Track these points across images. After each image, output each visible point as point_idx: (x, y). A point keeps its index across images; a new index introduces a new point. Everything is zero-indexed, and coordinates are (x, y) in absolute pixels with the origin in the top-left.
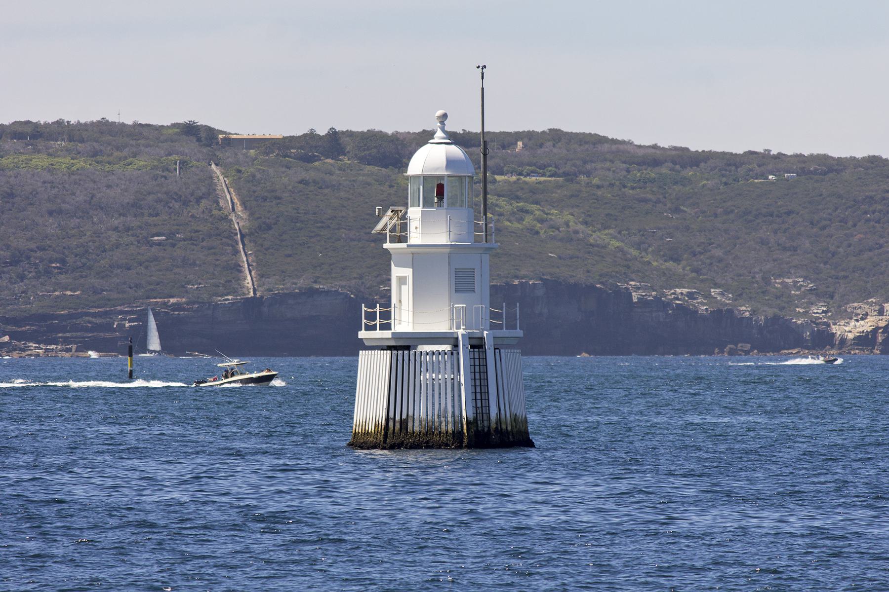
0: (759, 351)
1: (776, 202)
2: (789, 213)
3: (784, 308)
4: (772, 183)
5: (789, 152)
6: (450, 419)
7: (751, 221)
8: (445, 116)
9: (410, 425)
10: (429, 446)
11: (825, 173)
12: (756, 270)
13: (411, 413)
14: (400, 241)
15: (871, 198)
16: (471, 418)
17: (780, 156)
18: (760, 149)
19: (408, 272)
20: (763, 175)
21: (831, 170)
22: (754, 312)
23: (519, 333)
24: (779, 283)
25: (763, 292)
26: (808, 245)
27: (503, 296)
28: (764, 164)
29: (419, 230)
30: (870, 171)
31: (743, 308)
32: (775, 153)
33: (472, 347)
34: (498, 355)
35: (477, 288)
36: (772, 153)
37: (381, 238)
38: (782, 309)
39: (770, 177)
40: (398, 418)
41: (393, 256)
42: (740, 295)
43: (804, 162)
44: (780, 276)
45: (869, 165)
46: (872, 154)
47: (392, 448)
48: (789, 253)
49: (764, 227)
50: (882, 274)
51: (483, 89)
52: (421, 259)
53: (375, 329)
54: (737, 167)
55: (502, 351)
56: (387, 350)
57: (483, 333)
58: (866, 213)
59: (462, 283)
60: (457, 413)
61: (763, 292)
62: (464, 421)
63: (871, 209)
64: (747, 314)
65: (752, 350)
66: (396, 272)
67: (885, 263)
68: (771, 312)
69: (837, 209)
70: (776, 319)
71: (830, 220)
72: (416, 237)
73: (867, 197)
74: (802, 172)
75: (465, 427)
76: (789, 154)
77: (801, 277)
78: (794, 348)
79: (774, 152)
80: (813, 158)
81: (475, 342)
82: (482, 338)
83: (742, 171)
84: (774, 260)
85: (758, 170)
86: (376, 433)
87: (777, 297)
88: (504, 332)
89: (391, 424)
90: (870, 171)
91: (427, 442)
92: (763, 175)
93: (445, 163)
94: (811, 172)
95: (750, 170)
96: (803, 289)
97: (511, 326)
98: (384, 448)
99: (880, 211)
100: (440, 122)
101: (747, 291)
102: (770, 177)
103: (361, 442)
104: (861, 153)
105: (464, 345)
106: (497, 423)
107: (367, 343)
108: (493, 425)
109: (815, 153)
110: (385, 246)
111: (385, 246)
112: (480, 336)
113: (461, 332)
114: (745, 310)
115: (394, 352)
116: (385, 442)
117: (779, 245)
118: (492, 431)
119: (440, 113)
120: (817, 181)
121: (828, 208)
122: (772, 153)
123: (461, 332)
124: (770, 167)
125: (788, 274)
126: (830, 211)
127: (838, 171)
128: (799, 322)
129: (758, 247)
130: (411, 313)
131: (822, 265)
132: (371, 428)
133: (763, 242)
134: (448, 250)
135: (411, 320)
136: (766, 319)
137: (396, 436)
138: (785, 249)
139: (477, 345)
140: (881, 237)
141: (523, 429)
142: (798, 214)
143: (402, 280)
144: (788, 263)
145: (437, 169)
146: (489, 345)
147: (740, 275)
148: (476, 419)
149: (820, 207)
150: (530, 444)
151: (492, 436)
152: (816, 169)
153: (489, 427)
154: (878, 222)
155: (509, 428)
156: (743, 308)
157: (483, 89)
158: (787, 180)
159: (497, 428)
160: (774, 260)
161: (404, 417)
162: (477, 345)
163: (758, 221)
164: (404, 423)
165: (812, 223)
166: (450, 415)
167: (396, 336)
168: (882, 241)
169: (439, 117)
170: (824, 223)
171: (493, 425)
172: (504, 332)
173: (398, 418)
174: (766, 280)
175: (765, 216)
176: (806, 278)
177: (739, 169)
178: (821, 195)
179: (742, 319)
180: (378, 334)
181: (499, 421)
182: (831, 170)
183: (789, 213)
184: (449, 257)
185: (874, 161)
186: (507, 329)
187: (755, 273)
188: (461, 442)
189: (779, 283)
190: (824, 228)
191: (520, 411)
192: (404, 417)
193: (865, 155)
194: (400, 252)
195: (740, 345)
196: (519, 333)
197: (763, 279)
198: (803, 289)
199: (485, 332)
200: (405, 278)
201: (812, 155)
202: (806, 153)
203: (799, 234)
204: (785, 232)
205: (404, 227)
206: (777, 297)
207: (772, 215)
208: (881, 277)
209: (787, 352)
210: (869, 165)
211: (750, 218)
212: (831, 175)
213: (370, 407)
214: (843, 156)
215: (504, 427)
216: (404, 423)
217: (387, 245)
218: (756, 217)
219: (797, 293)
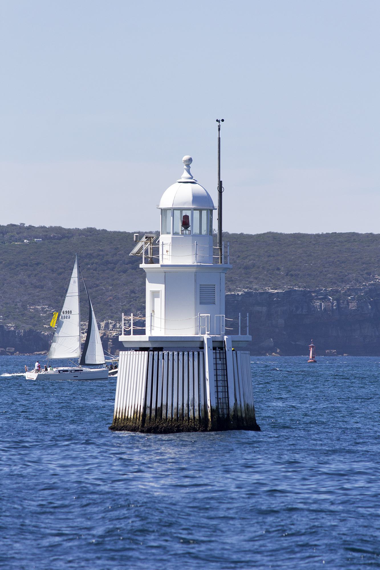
0: (20, 353)
1: (29, 257)
2: (37, 264)
3: (36, 325)
4: (27, 245)
5: (36, 225)
6: (197, 408)
7: (13, 269)
8: (190, 160)
9: (164, 412)
10: (179, 430)
11: (60, 239)
12: (18, 300)
13: (164, 403)
14: (152, 262)
15: (91, 255)
16: (214, 407)
17: (30, 228)
18: (18, 223)
19: (161, 288)
20: (21, 240)
21: (64, 237)
22: (16, 327)
23: (248, 337)
24: (32, 309)
25: (22, 315)
26: (50, 284)
27: (232, 306)
28: (20, 233)
29: (170, 253)
30: (89, 238)
31: (10, 325)
32: (28, 226)
33: (214, 349)
34: (235, 355)
35: (216, 302)
36: (25, 226)
37: (139, 260)
38: (35, 325)
39: (25, 241)
40: (154, 406)
41: (147, 275)
42: (8, 316)
43: (47, 232)
44: (33, 304)
45: (89, 233)
46: (89, 226)
47: (149, 431)
48: (38, 290)
49: (22, 273)
50: (98, 303)
51: (219, 138)
52: (172, 276)
53: (130, 334)
54: (4, 234)
55: (238, 352)
56: (139, 351)
57: (223, 338)
58: (87, 264)
59: (205, 297)
60: (202, 403)
61: (22, 315)
62: (209, 410)
63: (91, 262)
64: (12, 329)
65: (15, 352)
66: (150, 287)
67: (100, 296)
68: (28, 327)
69: (68, 261)
70: (31, 331)
71: (64, 269)
72: (167, 258)
73: (88, 254)
74: (45, 238)
75: (209, 414)
76: (36, 226)
77: (46, 305)
78: (42, 351)
79: (27, 225)
80: (52, 229)
81: (217, 345)
82: (223, 342)
83: (7, 237)
84: (29, 294)
85: (17, 236)
86: (135, 419)
87: (31, 318)
88: (239, 337)
89: (148, 411)
90: (89, 238)
91: (178, 427)
92: (21, 240)
93: (191, 199)
94: (50, 238)
95: (12, 236)
96: (48, 313)
97: (244, 333)
98: (142, 432)
99: (97, 263)
100: (186, 165)
101: (12, 314)
102: (25, 241)
103: (120, 425)
104: (82, 226)
105: (209, 347)
106: (234, 411)
107: (126, 346)
108: (232, 413)
109: (53, 225)
110: (141, 266)
111: (141, 266)
112: (221, 340)
113: (206, 337)
114: (11, 326)
115: (151, 353)
116: (143, 426)
117: (31, 284)
118: (231, 417)
119: (186, 157)
120: (55, 244)
121: (63, 261)
122: (25, 226)
123: (206, 337)
124: (25, 234)
125: (38, 303)
126: (64, 263)
127: (68, 238)
128: (46, 334)
129: (18, 286)
130: (163, 321)
131: (60, 298)
132: (130, 414)
133: (22, 283)
134: (194, 270)
135: (163, 326)
136: (25, 332)
137: (153, 423)
138: (36, 287)
139: (218, 347)
140: (98, 279)
141: (252, 415)
142: (43, 264)
143: (155, 294)
144: (38, 296)
145: (185, 203)
146: (229, 348)
147: (7, 304)
148: (217, 408)
149: (58, 260)
150: (257, 428)
151: (229, 421)
152: (54, 236)
153: (228, 414)
154: (95, 270)
155: (244, 415)
156: (10, 325)
157: (219, 138)
158: (36, 243)
159: (234, 415)
160: (29, 294)
161: (159, 405)
162: (218, 347)
163: (18, 269)
164: (159, 411)
165: (53, 271)
166: (197, 404)
167: (152, 339)
168: (98, 282)
169: (185, 161)
170: (60, 270)
171: (232, 413)
172: (239, 337)
173: (154, 406)
174: (24, 307)
175: (22, 266)
176: (50, 306)
177: (5, 236)
178: (58, 253)
179: (9, 331)
180: (133, 338)
181: (235, 410)
182: (64, 237)
183: (37, 264)
184: (195, 275)
185: (91, 231)
186: (133, 335)
187: (16, 302)
188: (206, 426)
189: (32, 309)
190: (60, 274)
191: (250, 402)
192: (159, 405)
193: (85, 227)
194: (155, 272)
195: (7, 348)
196: (248, 337)
197: (23, 306)
198: (48, 313)
199: (225, 337)
200: (158, 292)
201: (51, 227)
202: (47, 226)
203: (44, 277)
204: (35, 276)
205: (156, 251)
206: (31, 318)
207: (26, 265)
208: (98, 305)
209: (38, 353)
210: (89, 233)
211: (13, 267)
212: (64, 240)
213: (129, 395)
214: (71, 228)
215: (239, 414)
216: (159, 411)
217: (143, 266)
218: (17, 266)
219: (44, 315)
